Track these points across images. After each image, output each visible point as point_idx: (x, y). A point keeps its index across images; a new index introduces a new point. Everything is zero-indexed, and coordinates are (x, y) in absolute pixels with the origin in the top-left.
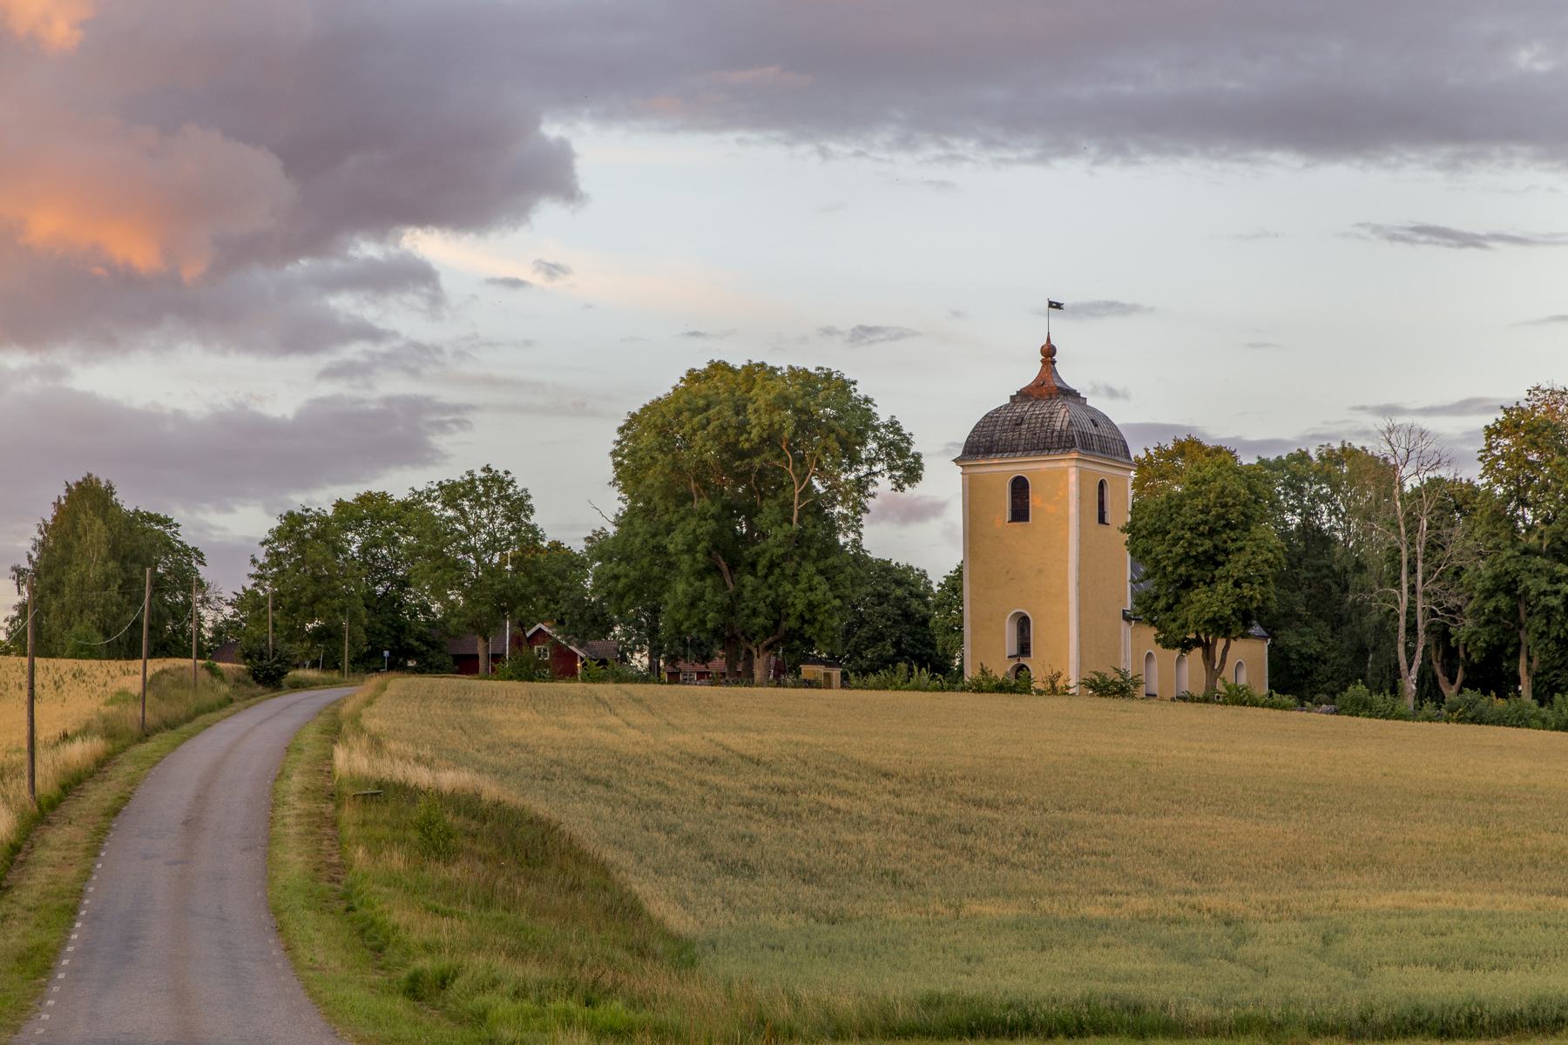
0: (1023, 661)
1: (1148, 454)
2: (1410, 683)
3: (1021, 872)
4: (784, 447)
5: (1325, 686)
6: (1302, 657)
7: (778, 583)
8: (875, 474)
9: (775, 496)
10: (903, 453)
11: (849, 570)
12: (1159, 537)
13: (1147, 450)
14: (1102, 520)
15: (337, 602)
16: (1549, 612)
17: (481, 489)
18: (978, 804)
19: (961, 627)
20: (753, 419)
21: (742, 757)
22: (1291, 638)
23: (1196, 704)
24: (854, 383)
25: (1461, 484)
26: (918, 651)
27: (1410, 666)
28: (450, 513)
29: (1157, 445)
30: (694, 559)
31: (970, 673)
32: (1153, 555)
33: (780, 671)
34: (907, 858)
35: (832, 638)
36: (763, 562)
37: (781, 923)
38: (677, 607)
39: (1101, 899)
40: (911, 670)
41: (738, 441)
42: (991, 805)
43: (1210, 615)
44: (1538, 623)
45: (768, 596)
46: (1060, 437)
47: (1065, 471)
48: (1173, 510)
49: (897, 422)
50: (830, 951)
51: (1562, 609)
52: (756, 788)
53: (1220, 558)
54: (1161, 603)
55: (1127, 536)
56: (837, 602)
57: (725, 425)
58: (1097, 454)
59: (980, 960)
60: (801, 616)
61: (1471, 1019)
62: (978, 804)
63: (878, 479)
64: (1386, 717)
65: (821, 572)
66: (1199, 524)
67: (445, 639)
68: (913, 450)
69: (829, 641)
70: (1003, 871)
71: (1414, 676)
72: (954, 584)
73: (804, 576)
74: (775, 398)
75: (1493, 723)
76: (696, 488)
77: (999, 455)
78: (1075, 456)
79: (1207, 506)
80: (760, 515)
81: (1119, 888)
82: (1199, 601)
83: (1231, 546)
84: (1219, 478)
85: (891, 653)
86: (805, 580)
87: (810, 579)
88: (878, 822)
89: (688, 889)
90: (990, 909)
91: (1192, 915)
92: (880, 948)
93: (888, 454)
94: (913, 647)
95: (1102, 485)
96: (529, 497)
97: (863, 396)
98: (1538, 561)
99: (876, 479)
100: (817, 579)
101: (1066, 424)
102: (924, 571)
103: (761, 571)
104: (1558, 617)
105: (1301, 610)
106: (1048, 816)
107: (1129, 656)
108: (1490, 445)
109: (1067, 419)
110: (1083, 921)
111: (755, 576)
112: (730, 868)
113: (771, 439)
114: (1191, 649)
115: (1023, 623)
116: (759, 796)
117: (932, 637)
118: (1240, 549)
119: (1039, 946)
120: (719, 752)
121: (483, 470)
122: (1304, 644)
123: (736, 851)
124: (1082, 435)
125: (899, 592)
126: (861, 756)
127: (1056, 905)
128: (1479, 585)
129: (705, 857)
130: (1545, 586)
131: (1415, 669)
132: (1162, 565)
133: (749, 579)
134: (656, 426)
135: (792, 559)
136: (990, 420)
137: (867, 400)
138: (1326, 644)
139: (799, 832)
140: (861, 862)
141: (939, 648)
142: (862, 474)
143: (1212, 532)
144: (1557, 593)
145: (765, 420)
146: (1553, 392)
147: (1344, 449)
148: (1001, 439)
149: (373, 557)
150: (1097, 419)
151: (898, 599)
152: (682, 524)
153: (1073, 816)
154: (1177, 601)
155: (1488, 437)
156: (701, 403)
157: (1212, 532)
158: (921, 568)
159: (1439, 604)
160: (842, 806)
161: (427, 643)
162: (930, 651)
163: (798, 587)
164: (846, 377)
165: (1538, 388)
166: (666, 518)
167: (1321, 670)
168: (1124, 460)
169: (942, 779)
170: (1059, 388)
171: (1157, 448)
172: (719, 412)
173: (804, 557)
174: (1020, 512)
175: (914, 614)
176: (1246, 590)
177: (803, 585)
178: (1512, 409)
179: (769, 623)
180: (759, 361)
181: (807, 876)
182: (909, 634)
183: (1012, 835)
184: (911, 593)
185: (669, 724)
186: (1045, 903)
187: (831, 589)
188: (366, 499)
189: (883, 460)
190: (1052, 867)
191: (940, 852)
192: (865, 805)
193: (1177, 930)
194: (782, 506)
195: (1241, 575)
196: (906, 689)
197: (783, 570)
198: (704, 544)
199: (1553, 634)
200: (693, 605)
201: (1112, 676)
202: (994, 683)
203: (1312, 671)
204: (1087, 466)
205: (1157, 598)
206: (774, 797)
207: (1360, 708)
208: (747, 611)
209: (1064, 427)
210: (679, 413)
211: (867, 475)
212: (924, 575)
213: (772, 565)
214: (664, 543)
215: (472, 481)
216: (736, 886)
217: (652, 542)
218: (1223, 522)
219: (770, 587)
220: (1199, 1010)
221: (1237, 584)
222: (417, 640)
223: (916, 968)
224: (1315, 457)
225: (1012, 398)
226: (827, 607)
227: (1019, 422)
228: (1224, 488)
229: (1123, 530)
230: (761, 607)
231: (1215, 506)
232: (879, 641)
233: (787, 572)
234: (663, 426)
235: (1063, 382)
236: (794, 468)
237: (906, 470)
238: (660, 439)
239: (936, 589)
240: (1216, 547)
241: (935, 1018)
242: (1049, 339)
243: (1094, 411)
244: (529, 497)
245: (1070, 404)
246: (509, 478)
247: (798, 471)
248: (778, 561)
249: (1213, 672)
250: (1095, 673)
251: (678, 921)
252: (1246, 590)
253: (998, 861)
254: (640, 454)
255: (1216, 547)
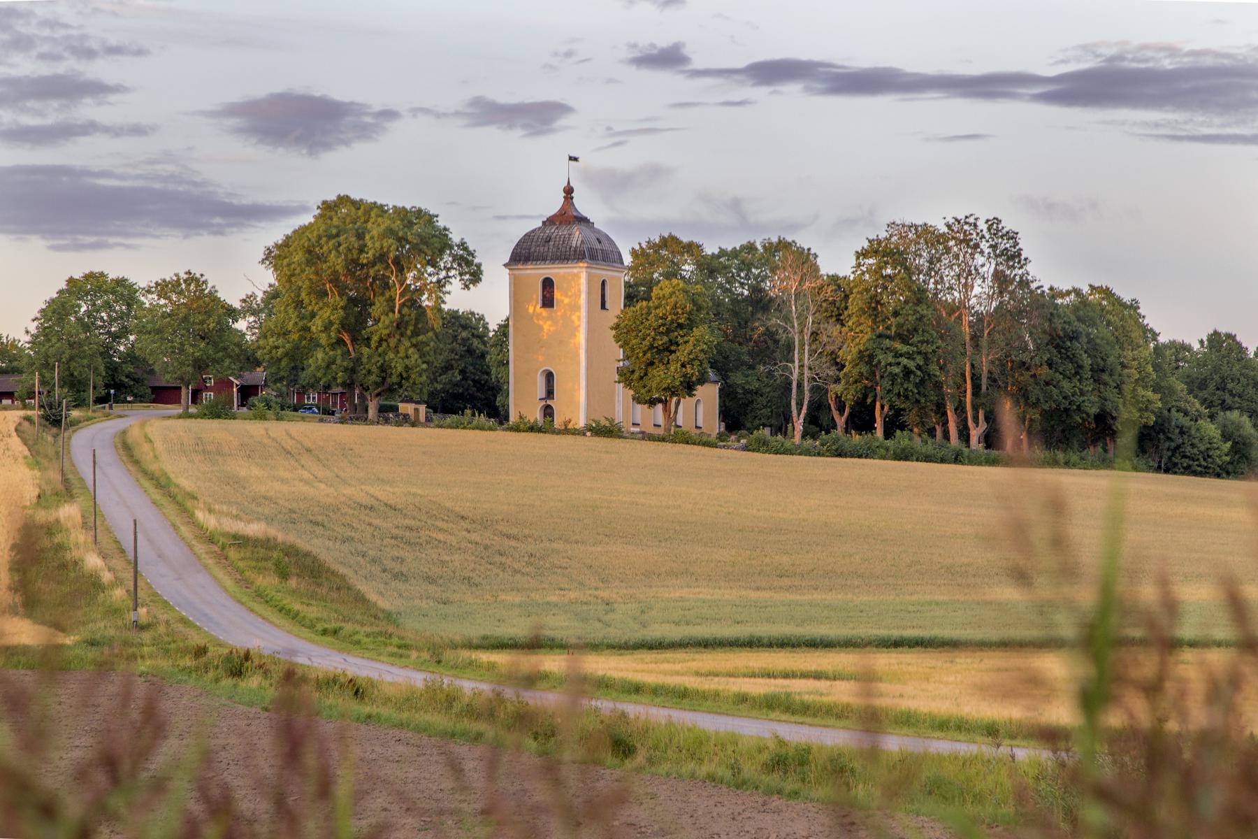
0: (549, 402)
1: (641, 247)
2: (799, 424)
3: (525, 578)
4: (390, 262)
5: (762, 412)
6: (746, 392)
7: (385, 353)
8: (449, 277)
9: (383, 294)
10: (469, 264)
11: (432, 344)
12: (634, 334)
13: (640, 244)
14: (603, 306)
15: (85, 362)
16: (893, 377)
17: (183, 286)
18: (508, 537)
19: (508, 362)
20: (369, 244)
21: (386, 504)
22: (738, 378)
23: (656, 443)
24: (437, 216)
25: (849, 280)
26: (477, 377)
27: (799, 415)
28: (162, 302)
29: (647, 240)
30: (329, 336)
31: (513, 418)
32: (630, 346)
33: (383, 410)
34: (473, 570)
35: (421, 390)
36: (375, 338)
37: (423, 604)
38: (318, 368)
39: (557, 592)
40: (473, 415)
41: (359, 258)
42: (515, 538)
43: (666, 385)
44: (886, 384)
45: (378, 361)
46: (575, 251)
47: (577, 276)
48: (644, 316)
49: (465, 243)
50: (445, 617)
51: (901, 375)
52: (397, 527)
53: (673, 348)
54: (636, 375)
55: (614, 332)
56: (424, 366)
57: (351, 247)
58: (600, 262)
59: (503, 621)
60: (401, 375)
61: (660, 644)
62: (508, 537)
63: (452, 280)
64: (777, 452)
65: (414, 346)
66: (660, 326)
67: (145, 376)
68: (476, 261)
69: (418, 391)
70: (518, 576)
71: (801, 420)
72: (504, 329)
73: (402, 349)
74: (384, 230)
75: (852, 456)
76: (330, 288)
77: (534, 263)
78: (586, 265)
79: (665, 314)
80: (373, 307)
81: (567, 587)
82: (659, 376)
83: (680, 340)
84: (673, 296)
85: (458, 379)
86: (403, 351)
87: (407, 350)
88: (460, 549)
89: (382, 587)
90: (510, 598)
91: (593, 600)
92: (465, 616)
93: (459, 265)
94: (474, 374)
95: (603, 283)
96: (216, 291)
97: (442, 226)
98: (887, 342)
99: (451, 280)
100: (411, 351)
101: (579, 242)
102: (483, 316)
103: (373, 344)
104: (899, 380)
105: (746, 358)
106: (542, 545)
107: (621, 398)
108: (860, 263)
109: (580, 239)
110: (548, 603)
111: (369, 347)
112: (398, 576)
113: (381, 257)
114: (655, 405)
115: (549, 376)
116: (399, 532)
117: (488, 367)
118: (686, 342)
119: (527, 615)
120: (374, 503)
121: (186, 273)
122: (747, 382)
123: (397, 567)
124: (590, 250)
125: (464, 334)
126: (449, 504)
127: (538, 596)
128: (849, 358)
129: (384, 571)
130: (890, 360)
131: (802, 416)
132: (636, 352)
133: (365, 351)
134: (304, 247)
135: (394, 337)
136: (528, 237)
137: (445, 229)
138: (763, 382)
139: (424, 555)
140: (454, 572)
141: (493, 377)
142: (441, 277)
143: (668, 331)
144: (899, 364)
145: (378, 245)
146: (903, 226)
147: (780, 241)
148: (535, 251)
149: (95, 318)
150: (602, 238)
151: (463, 339)
152: (320, 313)
153: (555, 545)
154: (646, 374)
155: (858, 258)
156: (334, 231)
157: (668, 331)
158: (481, 313)
159: (817, 374)
160: (442, 539)
161: (134, 380)
162: (486, 377)
163: (399, 355)
164: (431, 213)
165: (894, 223)
166: (310, 308)
167: (759, 400)
168: (620, 265)
169: (492, 521)
170: (575, 217)
171: (648, 242)
172: (346, 239)
173: (402, 335)
174: (548, 302)
175: (475, 351)
176: (689, 370)
177: (402, 354)
178: (873, 240)
179: (379, 380)
180: (373, 201)
181: (430, 580)
182: (472, 365)
183: (524, 557)
184: (473, 335)
185: (337, 477)
186: (533, 595)
187: (420, 357)
188: (90, 276)
189: (456, 269)
190: (540, 575)
191: (489, 567)
192: (453, 538)
193: (585, 608)
194: (387, 301)
195: (686, 359)
196: (470, 429)
197: (388, 344)
198: (336, 326)
199: (896, 391)
200: (328, 367)
201: (604, 422)
202: (528, 425)
203: (752, 401)
204: (593, 271)
205: (633, 372)
206: (408, 534)
207: (761, 446)
208: (364, 372)
209: (578, 245)
210: (320, 237)
211: (445, 278)
212: (482, 318)
213: (381, 340)
214: (309, 325)
215: (179, 279)
216: (400, 585)
217: (301, 324)
218: (675, 325)
219: (380, 355)
220: (573, 641)
221: (683, 366)
222: (127, 377)
223: (479, 625)
224: (759, 247)
225: (544, 223)
226: (418, 369)
227: (548, 240)
228: (676, 303)
229: (612, 328)
230: (374, 369)
231: (670, 314)
232: (450, 370)
233: (391, 345)
234: (309, 246)
235: (578, 212)
236: (397, 276)
237: (471, 274)
238: (307, 255)
239: (491, 334)
240: (670, 341)
241: (485, 643)
242: (569, 182)
243: (599, 231)
244: (216, 291)
245: (583, 227)
246: (204, 279)
247: (399, 278)
248: (385, 338)
249: (670, 417)
250: (593, 420)
251: (384, 604)
252: (689, 370)
253: (516, 571)
254: (293, 266)
255: (670, 341)
